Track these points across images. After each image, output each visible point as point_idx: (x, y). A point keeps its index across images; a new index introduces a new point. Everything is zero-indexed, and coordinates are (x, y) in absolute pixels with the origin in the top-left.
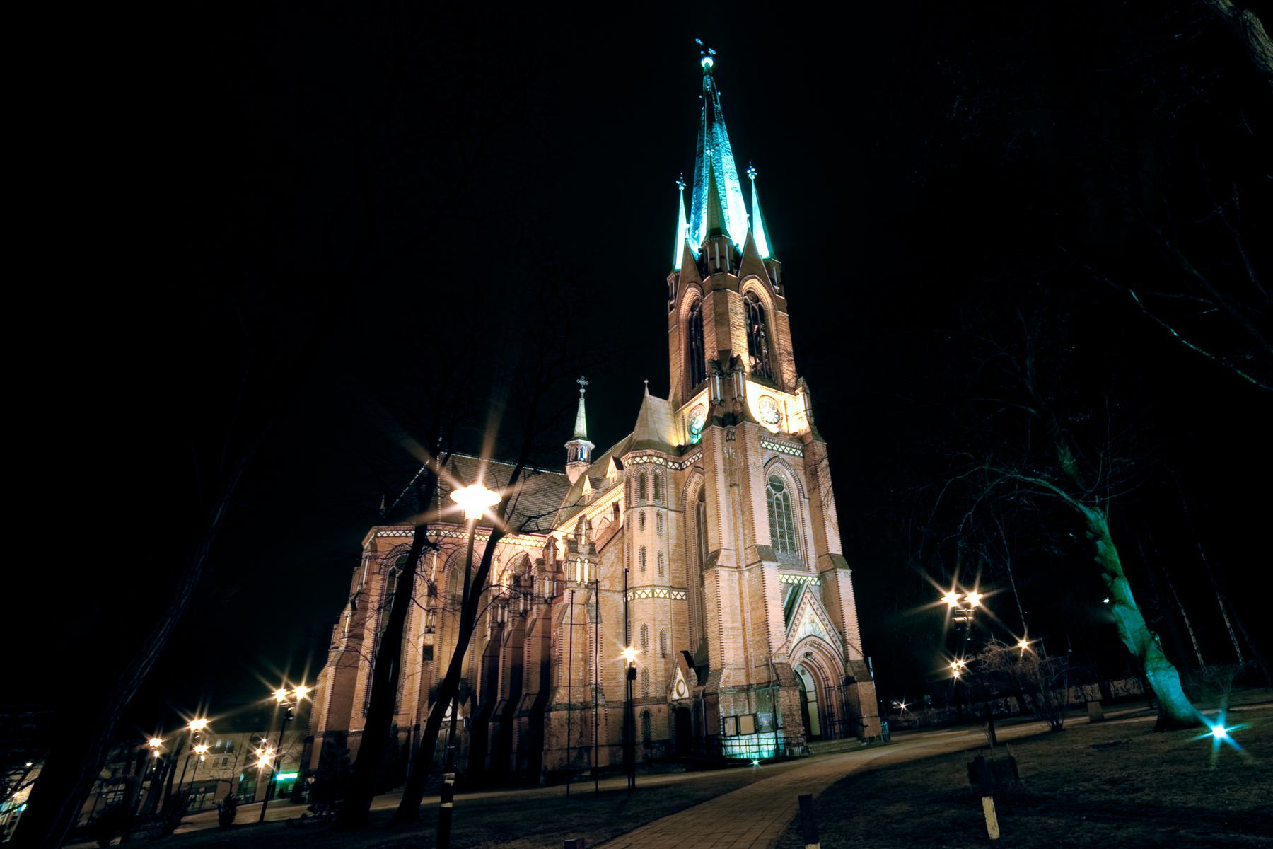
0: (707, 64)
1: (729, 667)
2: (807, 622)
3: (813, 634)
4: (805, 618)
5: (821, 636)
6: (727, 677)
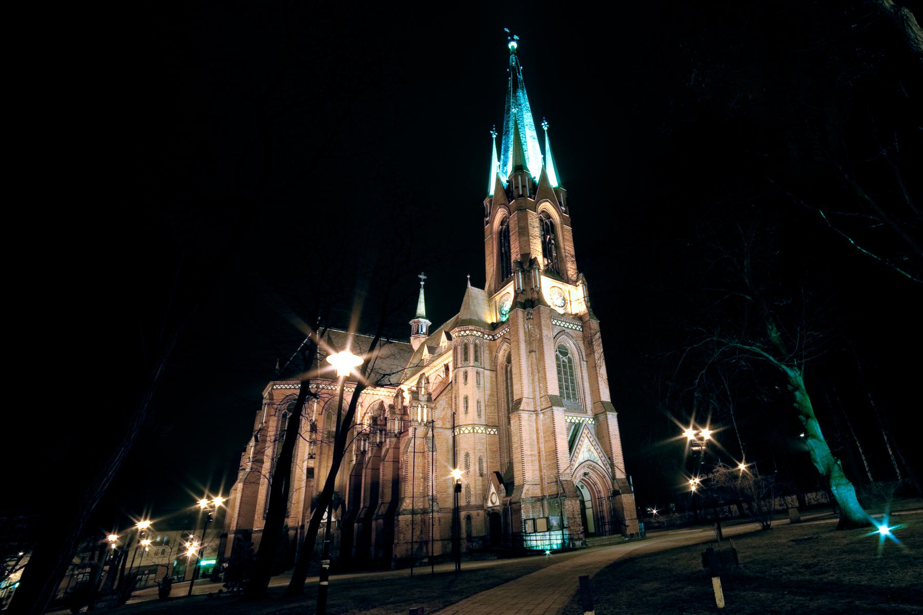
0: (513, 47)
1: (529, 483)
2: (585, 450)
3: (589, 459)
4: (584, 448)
5: (595, 461)
6: (527, 490)
